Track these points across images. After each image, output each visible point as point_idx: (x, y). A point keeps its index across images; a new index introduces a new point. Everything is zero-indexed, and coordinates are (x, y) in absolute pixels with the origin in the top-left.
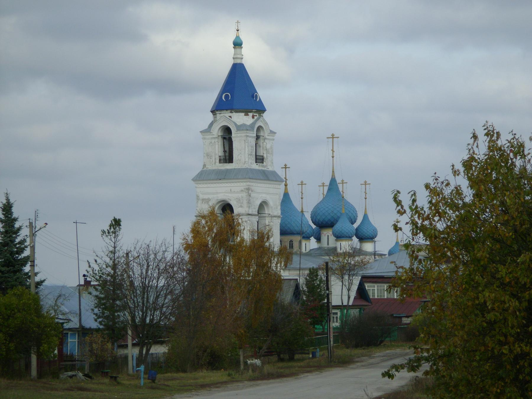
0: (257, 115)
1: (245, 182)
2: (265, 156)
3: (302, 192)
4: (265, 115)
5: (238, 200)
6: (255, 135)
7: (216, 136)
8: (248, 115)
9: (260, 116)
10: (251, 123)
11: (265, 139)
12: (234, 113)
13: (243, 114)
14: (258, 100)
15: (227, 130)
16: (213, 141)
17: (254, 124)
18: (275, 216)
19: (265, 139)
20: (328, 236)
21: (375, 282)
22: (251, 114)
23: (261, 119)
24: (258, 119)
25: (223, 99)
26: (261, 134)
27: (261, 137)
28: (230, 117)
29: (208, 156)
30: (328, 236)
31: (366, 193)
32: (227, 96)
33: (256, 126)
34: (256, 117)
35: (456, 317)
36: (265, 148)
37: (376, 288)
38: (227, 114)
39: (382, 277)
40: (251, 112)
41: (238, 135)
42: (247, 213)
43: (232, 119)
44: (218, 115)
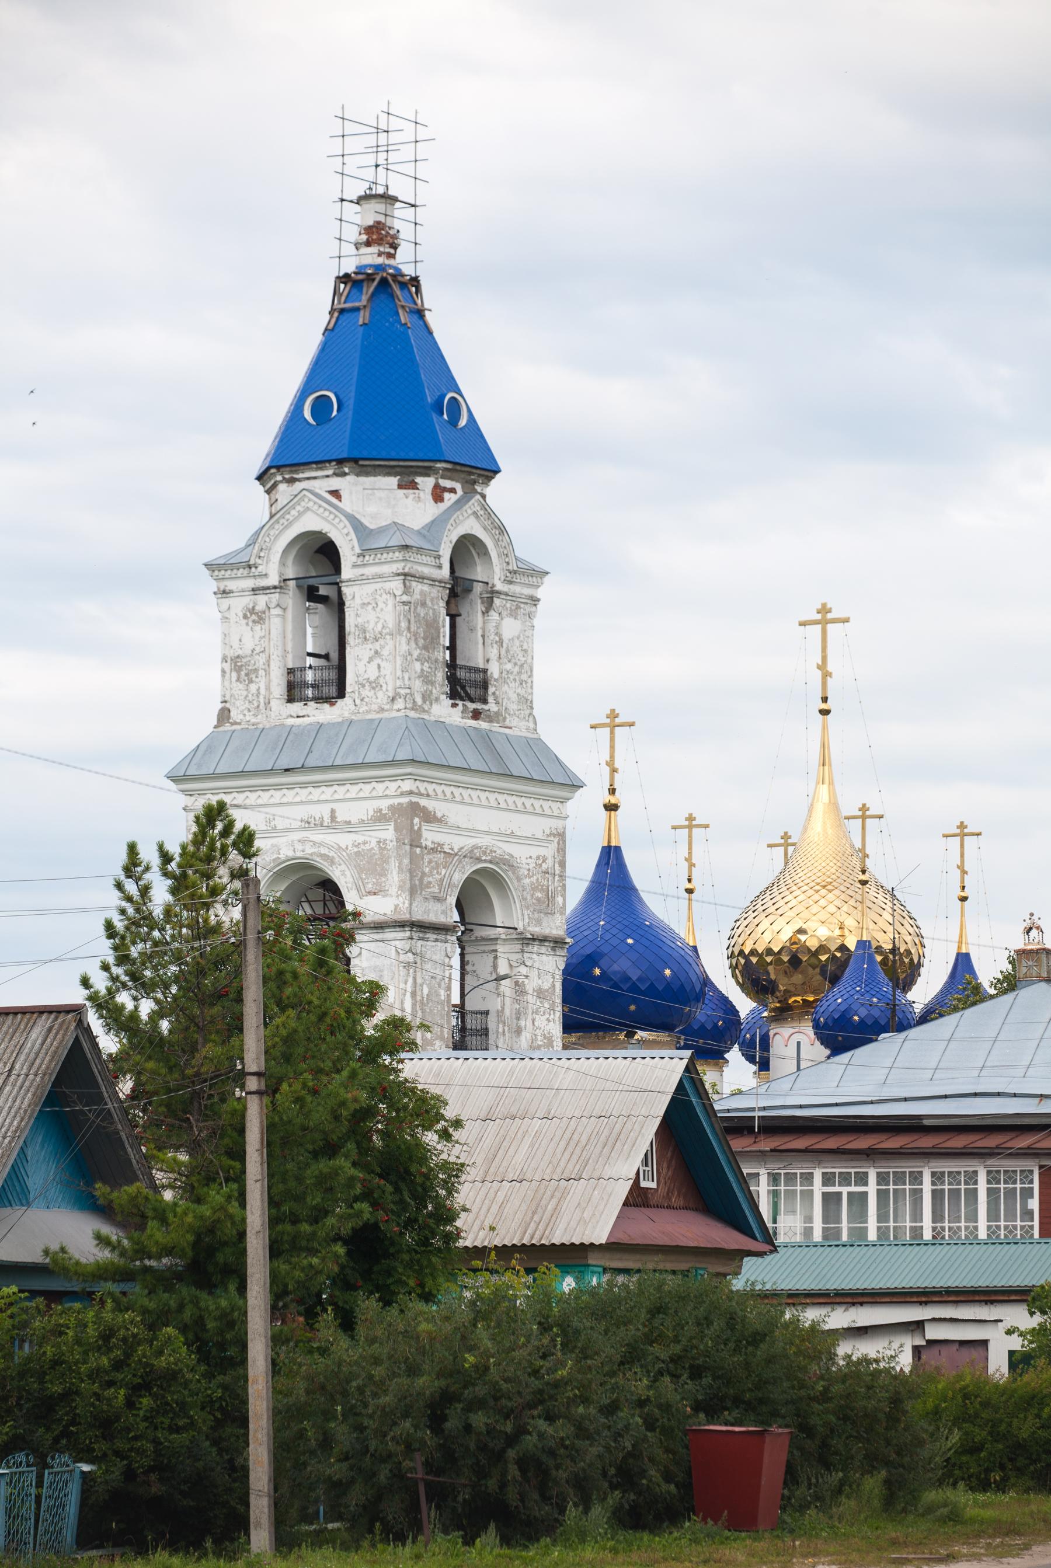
0: (458, 486)
1: (392, 778)
2: (494, 670)
3: (689, 859)
4: (495, 492)
5: (372, 865)
6: (445, 572)
7: (273, 580)
8: (413, 486)
9: (470, 490)
10: (428, 519)
11: (490, 597)
12: (350, 478)
13: (393, 481)
14: (463, 422)
15: (322, 552)
16: (262, 600)
17: (436, 526)
18: (542, 940)
19: (490, 597)
20: (799, 1043)
21: (870, 1155)
22: (426, 483)
23: (474, 502)
24: (459, 504)
25: (307, 414)
26: (479, 572)
27: (478, 588)
28: (335, 493)
29: (238, 669)
30: (799, 1043)
31: (964, 872)
32: (321, 404)
33: (453, 536)
34: (449, 498)
35: (156, 1428)
36: (492, 637)
37: (872, 1189)
38: (322, 482)
39: (912, 1126)
40: (426, 472)
41: (369, 571)
42: (406, 917)
43: (346, 504)
44: (282, 487)
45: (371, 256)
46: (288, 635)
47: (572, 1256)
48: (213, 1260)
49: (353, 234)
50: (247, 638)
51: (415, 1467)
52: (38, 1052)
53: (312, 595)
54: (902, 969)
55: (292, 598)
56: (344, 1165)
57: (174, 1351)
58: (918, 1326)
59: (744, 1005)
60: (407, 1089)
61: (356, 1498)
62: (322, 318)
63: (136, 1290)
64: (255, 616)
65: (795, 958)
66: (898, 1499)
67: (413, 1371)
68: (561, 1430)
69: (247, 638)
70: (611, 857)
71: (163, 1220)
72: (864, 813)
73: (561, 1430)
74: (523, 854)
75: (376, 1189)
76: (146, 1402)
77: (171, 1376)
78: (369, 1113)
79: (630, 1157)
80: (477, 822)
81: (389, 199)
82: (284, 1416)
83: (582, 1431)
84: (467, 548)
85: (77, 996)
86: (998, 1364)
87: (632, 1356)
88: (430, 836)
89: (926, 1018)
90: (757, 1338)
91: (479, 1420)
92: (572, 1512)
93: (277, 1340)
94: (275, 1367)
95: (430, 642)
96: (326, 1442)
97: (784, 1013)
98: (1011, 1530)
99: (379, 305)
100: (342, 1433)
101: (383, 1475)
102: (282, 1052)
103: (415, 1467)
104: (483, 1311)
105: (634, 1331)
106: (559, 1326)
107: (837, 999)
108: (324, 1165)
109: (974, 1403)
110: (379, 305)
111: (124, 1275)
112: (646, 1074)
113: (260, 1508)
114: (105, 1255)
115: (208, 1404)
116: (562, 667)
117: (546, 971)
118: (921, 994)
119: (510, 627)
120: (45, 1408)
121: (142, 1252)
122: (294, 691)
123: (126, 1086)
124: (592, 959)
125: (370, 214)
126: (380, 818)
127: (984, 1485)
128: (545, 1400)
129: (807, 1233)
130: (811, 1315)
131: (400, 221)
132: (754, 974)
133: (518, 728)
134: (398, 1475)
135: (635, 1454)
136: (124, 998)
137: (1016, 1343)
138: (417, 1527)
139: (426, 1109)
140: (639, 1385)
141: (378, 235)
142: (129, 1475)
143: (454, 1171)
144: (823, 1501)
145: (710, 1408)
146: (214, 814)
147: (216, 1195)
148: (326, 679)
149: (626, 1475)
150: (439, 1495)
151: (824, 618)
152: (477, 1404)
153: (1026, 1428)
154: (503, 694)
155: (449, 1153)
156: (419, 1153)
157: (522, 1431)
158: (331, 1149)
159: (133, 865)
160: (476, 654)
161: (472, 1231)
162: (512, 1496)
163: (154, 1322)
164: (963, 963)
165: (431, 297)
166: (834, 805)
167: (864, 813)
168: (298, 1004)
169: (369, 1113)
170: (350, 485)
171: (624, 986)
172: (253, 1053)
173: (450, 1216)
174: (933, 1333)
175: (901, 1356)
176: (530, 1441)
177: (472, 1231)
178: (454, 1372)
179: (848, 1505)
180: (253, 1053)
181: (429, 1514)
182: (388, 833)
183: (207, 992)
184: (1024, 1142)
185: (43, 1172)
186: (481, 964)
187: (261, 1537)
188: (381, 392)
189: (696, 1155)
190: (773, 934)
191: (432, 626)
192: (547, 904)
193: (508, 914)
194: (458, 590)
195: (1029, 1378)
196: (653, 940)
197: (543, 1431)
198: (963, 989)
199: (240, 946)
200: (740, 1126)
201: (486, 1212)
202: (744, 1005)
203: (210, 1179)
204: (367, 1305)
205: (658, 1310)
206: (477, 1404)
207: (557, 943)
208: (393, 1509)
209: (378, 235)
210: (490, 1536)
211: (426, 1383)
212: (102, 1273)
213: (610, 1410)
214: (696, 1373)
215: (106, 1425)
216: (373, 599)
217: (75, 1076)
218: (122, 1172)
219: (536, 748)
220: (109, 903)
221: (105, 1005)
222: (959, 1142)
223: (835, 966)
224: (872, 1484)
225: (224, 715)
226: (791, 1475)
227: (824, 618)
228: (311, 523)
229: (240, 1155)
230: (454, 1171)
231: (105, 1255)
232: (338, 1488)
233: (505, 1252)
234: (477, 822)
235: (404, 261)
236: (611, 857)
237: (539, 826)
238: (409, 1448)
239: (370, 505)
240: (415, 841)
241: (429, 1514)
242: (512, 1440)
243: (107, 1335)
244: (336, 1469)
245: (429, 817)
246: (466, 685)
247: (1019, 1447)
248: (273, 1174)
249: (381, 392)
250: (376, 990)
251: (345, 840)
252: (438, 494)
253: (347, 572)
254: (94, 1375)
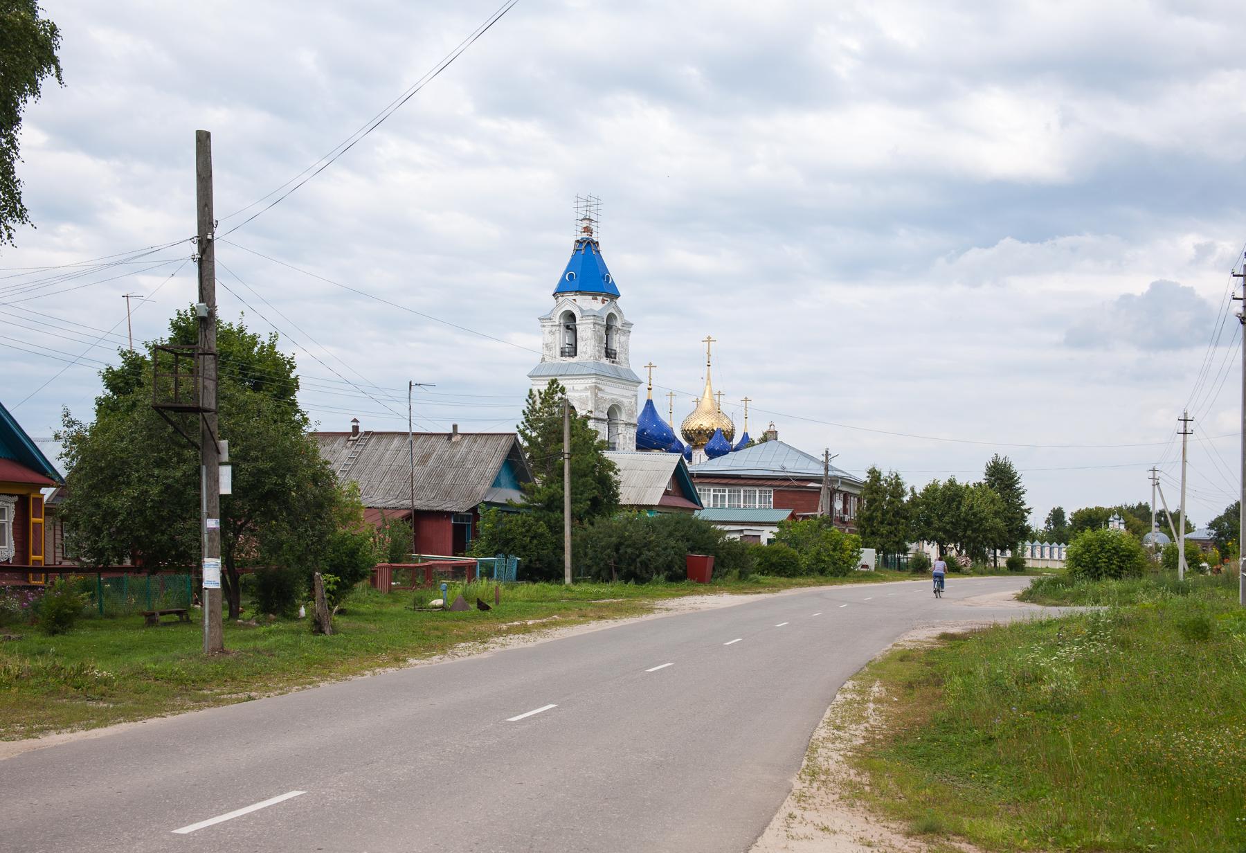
4: (619, 301)
9: (612, 300)
15: (571, 316)
21: (726, 485)
22: (600, 298)
38: (571, 297)
45: (585, 235)
46: (560, 339)
47: (649, 508)
48: (554, 504)
49: (580, 229)
50: (549, 339)
51: (611, 562)
52: (504, 446)
53: (568, 327)
54: (729, 436)
55: (562, 329)
56: (590, 479)
57: (542, 528)
58: (742, 531)
59: (685, 444)
60: (605, 460)
61: (594, 569)
62: (572, 252)
63: (532, 511)
64: (552, 333)
65: (700, 432)
66: (743, 576)
67: (610, 536)
68: (652, 554)
69: (549, 339)
70: (649, 402)
71: (539, 492)
72: (719, 394)
73: (652, 554)
74: (626, 401)
75: (599, 489)
76: (535, 541)
77: (542, 535)
78: (595, 466)
79: (665, 482)
80: (613, 392)
81: (590, 220)
82: (573, 546)
83: (658, 555)
84: (611, 317)
85: (515, 431)
86: (764, 541)
87: (670, 535)
88: (600, 395)
89: (736, 449)
90: (705, 532)
91: (629, 550)
92: (655, 577)
93: (572, 526)
94: (572, 534)
95: (601, 342)
96: (586, 554)
97: (696, 447)
98: (774, 586)
99: (587, 250)
100: (590, 551)
101: (602, 564)
102: (574, 448)
103: (611, 562)
104: (630, 521)
105: (670, 528)
106: (651, 526)
107: (711, 443)
108: (584, 479)
109: (760, 550)
110: (587, 250)
111: (529, 508)
112: (669, 461)
113: (568, 572)
114: (523, 501)
115: (552, 543)
116: (637, 347)
117: (633, 432)
118: (736, 440)
119: (623, 339)
120: (507, 542)
121: (533, 501)
122: (563, 354)
123: (527, 455)
124: (644, 430)
125: (585, 224)
126: (586, 389)
127: (763, 574)
128: (647, 545)
129: (713, 506)
130: (719, 527)
131: (593, 226)
132: (688, 435)
133: (625, 366)
134: (606, 564)
135: (671, 561)
136: (528, 432)
137: (771, 536)
138: (611, 578)
139: (611, 466)
140: (673, 543)
141: (587, 230)
142: (531, 561)
143: (618, 483)
144: (722, 576)
145: (692, 550)
146: (554, 382)
147: (554, 486)
148: (573, 351)
149: (669, 567)
150: (618, 570)
151: (650, 366)
152: (628, 546)
153: (774, 559)
154: (620, 357)
155: (617, 478)
156: (609, 477)
157: (641, 554)
158: (585, 475)
159: (531, 395)
160: (615, 346)
161: (623, 500)
162: (638, 571)
163: (537, 520)
164: (746, 436)
165: (601, 247)
166: (711, 391)
167: (719, 394)
168: (579, 436)
169: (595, 466)
170: (579, 298)
171: (652, 437)
172: (566, 449)
173: (617, 495)
174: (746, 533)
175: (737, 536)
176: (643, 557)
177: (623, 500)
178: (622, 537)
179: (729, 577)
180: (566, 449)
181: (615, 575)
182: (589, 394)
183: (552, 432)
184: (769, 483)
185: (505, 479)
186: (613, 430)
187: (568, 580)
188: (587, 273)
189: (683, 482)
190: (694, 425)
191: (601, 338)
192: (631, 415)
193: (623, 417)
194: (609, 328)
195: (775, 546)
196: (661, 426)
197: (647, 554)
198: (747, 442)
199: (562, 419)
200: (692, 475)
201: (627, 495)
202: (685, 444)
203: (552, 482)
204: (598, 518)
205: (678, 523)
206: (628, 546)
207: (635, 425)
208: (604, 574)
209: (587, 230)
210: (632, 583)
211: (614, 540)
212: (523, 506)
213: (665, 549)
214: (688, 540)
215: (524, 547)
216: (585, 330)
217: (515, 450)
218: (527, 480)
219: (629, 371)
220: (524, 406)
221: (523, 433)
222: (751, 482)
223: (711, 434)
224: (736, 572)
225: (543, 360)
226: (714, 569)
227: (650, 366)
228: (568, 308)
229: (562, 476)
230: (618, 483)
231: (523, 501)
232: (589, 567)
233: (632, 506)
234: (613, 392)
235: (594, 237)
236: (649, 402)
237: (630, 393)
238: (609, 558)
239: (585, 305)
240: (596, 395)
241: (615, 575)
242: (638, 556)
243: (524, 523)
244: (588, 562)
245: (600, 390)
246: (610, 354)
247: (772, 564)
248: (572, 482)
249: (587, 273)
250: (597, 433)
251: (577, 395)
252: (603, 301)
253: (578, 322)
254: (521, 533)
